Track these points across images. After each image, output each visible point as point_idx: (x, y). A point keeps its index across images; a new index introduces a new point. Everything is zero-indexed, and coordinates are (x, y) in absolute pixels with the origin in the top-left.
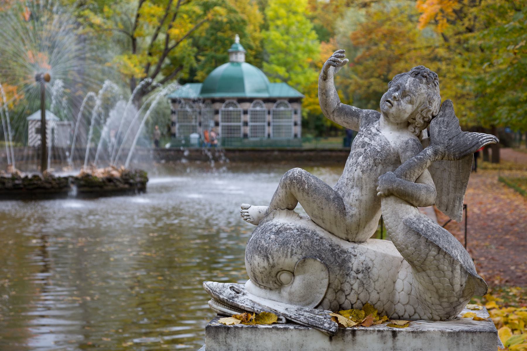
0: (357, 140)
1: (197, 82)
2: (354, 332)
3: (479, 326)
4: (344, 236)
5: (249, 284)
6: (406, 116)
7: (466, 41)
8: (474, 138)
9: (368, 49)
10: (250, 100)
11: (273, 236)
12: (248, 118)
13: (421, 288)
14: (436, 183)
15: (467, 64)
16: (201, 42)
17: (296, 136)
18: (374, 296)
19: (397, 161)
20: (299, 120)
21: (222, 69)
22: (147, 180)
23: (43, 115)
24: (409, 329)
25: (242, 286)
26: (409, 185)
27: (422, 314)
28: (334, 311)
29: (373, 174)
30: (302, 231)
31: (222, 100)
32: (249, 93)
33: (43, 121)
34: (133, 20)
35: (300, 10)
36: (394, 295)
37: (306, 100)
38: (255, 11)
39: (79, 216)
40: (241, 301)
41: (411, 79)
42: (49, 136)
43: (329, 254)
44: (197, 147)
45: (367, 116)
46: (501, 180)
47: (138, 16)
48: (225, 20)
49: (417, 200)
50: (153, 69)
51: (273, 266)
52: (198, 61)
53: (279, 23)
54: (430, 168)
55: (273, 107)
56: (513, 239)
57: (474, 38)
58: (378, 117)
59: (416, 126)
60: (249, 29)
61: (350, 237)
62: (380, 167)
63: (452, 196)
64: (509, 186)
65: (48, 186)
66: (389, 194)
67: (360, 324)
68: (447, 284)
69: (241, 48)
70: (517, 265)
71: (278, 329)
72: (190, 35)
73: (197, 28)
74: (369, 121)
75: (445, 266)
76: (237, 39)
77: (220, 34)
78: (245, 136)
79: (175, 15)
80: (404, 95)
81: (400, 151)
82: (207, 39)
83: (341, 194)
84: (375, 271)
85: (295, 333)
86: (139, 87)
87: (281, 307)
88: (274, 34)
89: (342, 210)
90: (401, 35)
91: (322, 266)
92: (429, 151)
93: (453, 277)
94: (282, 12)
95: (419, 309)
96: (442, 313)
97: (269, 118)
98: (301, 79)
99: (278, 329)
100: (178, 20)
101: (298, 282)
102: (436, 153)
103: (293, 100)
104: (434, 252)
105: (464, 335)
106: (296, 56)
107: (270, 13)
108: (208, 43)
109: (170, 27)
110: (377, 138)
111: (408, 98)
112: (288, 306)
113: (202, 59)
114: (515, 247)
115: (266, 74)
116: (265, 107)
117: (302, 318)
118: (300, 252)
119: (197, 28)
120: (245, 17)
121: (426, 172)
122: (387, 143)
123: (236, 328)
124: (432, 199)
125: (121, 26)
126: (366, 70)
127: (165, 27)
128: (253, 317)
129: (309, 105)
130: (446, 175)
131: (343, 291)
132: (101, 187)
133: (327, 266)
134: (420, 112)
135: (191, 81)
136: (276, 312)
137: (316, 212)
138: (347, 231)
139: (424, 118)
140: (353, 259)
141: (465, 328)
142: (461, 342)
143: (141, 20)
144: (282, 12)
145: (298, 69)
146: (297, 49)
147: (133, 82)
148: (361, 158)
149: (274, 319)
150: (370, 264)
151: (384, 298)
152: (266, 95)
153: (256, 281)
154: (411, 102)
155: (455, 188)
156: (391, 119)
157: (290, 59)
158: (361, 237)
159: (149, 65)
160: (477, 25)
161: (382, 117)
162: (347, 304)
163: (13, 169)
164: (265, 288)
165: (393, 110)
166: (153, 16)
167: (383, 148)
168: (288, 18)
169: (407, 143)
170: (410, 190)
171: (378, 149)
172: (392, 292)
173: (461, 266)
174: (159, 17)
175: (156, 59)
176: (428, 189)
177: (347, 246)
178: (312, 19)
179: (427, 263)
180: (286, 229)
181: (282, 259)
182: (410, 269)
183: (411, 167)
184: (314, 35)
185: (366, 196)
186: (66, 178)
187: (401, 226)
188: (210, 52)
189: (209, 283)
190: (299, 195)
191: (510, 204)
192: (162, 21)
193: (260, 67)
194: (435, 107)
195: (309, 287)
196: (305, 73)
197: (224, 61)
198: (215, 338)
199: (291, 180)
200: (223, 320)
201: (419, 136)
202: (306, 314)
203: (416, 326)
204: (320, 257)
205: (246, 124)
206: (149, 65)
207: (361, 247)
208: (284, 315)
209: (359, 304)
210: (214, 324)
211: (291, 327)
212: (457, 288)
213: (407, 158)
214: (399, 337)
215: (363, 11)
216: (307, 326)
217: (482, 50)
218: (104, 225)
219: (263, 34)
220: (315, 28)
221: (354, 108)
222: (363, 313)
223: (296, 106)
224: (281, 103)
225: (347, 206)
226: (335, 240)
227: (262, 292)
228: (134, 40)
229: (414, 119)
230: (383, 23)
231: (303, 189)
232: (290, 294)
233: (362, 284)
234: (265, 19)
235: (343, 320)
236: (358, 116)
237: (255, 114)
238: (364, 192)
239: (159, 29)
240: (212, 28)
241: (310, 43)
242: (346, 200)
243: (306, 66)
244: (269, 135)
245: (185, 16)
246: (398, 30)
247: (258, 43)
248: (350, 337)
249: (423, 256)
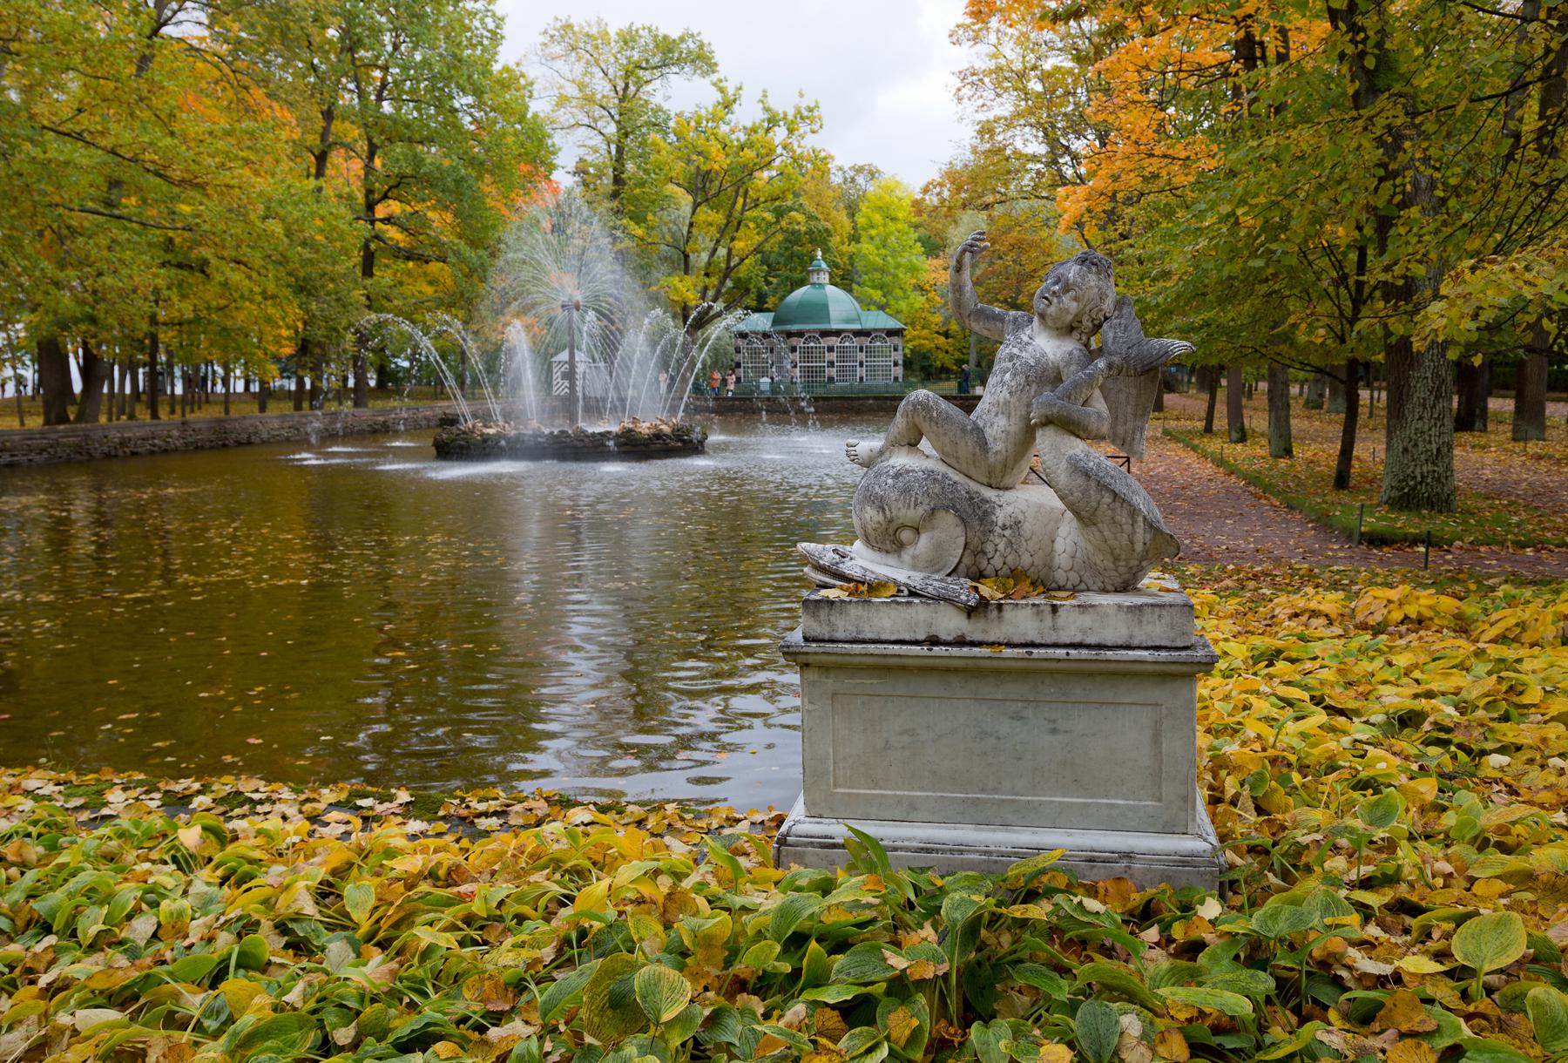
0: (1003, 352)
1: (768, 310)
2: (1000, 607)
3: (1168, 598)
4: (985, 480)
5: (858, 544)
6: (1070, 317)
7: (1120, 251)
8: (1161, 346)
9: (992, 264)
10: (837, 333)
11: (890, 481)
12: (833, 356)
13: (1089, 547)
14: (1110, 409)
15: (1121, 283)
16: (772, 258)
17: (896, 379)
18: (1026, 560)
19: (1057, 379)
20: (900, 358)
21: (800, 293)
23: (572, 355)
24: (1074, 602)
25: (848, 548)
26: (1075, 409)
27: (1090, 583)
28: (973, 579)
29: (1024, 397)
30: (929, 473)
31: (800, 334)
32: (835, 326)
33: (572, 362)
34: (685, 232)
35: (901, 215)
36: (1052, 559)
37: (910, 333)
38: (843, 217)
39: (621, 480)
40: (847, 568)
41: (1076, 268)
42: (579, 383)
43: (966, 504)
44: (768, 395)
45: (1016, 319)
46: (1166, 433)
47: (691, 225)
48: (803, 229)
49: (1085, 430)
50: (711, 293)
51: (891, 521)
52: (768, 283)
53: (873, 232)
54: (1101, 388)
55: (866, 341)
56: (1186, 505)
57: (1131, 246)
58: (1031, 321)
60: (834, 241)
61: (993, 482)
62: (1034, 387)
63: (1130, 425)
64: (1178, 441)
65: (579, 444)
66: (1048, 422)
67: (1008, 596)
68: (1125, 542)
69: (824, 265)
70: (1193, 537)
71: (898, 603)
72: (758, 250)
73: (767, 240)
74: (1018, 326)
75: (1123, 518)
76: (819, 253)
77: (796, 248)
78: (831, 379)
79: (739, 223)
80: (1067, 288)
81: (1062, 365)
82: (781, 255)
83: (981, 424)
84: (1027, 527)
85: (921, 608)
86: (693, 314)
87: (901, 575)
88: (866, 247)
89: (983, 444)
90: (1033, 245)
91: (956, 520)
92: (1101, 364)
93: (1134, 532)
94: (878, 218)
95: (1087, 576)
96: (1118, 581)
97: (861, 356)
98: (903, 305)
99: (898, 603)
100: (742, 228)
101: (924, 541)
102: (1110, 366)
103: (891, 333)
104: (1107, 499)
105: (1149, 610)
106: (895, 276)
107: (861, 220)
108: (782, 260)
109: (733, 239)
110: (1030, 348)
111: (1072, 293)
112: (912, 573)
113: (774, 280)
114: (1189, 515)
115: (856, 298)
116: (857, 341)
117: (930, 589)
118: (926, 501)
119: (767, 240)
120: (830, 226)
121: (1097, 393)
122: (1044, 355)
123: (843, 602)
124: (1105, 429)
125: (669, 238)
126: (988, 291)
127: (726, 240)
128: (864, 588)
129: (914, 338)
130: (1122, 397)
131: (985, 553)
132: (647, 446)
133: (962, 520)
135: (759, 309)
136: (895, 582)
137: (948, 449)
138: (990, 474)
140: (998, 511)
141: (1150, 600)
142: (1144, 619)
143: (695, 230)
144: (878, 218)
145: (900, 293)
146: (898, 266)
147: (685, 310)
148: (1008, 376)
149: (893, 591)
150: (1021, 517)
151: (1038, 561)
152: (857, 326)
153: (867, 541)
154: (1076, 299)
155: (1135, 415)
156: (1049, 322)
157: (888, 279)
158: (1007, 481)
159: (706, 288)
160: (1135, 230)
161: (1036, 319)
162: (989, 570)
163: (534, 424)
164: (880, 550)
165: (1052, 309)
166: (711, 225)
167: (1038, 362)
168: (885, 225)
169: (1071, 354)
170: (1075, 416)
171: (1032, 362)
172: (1050, 555)
173: (1145, 518)
174: (718, 227)
175: (714, 281)
176: (1099, 415)
177: (989, 494)
178: (916, 227)
179: (1099, 513)
180: (908, 472)
181: (903, 511)
182: (1075, 523)
183: (1076, 386)
184: (919, 248)
185: (1015, 426)
186: (602, 435)
187: (1064, 465)
188: (784, 272)
189: (805, 544)
190: (925, 426)
191: (1179, 462)
192: (722, 232)
193: (850, 291)
194: (1108, 305)
195: (939, 548)
196: (907, 298)
197: (802, 283)
198: (814, 615)
199: (914, 406)
200: (824, 593)
201: (1087, 345)
202: (936, 584)
203: (1083, 598)
204: (954, 507)
205: (831, 364)
206: (706, 288)
207: (1007, 496)
208: (906, 585)
209: (1005, 570)
210: (813, 597)
211: (917, 601)
212: (1139, 547)
213: (1072, 374)
214: (1061, 612)
215: (984, 215)
216: (938, 598)
217: (1141, 262)
219: (853, 248)
220: (919, 240)
221: (997, 310)
222: (1012, 582)
223: (896, 340)
225: (990, 440)
226: (974, 486)
227: (876, 556)
228: (686, 257)
230: (1010, 229)
231: (931, 418)
232: (914, 557)
233: (1010, 543)
234: (854, 228)
235: (985, 590)
236: (1002, 320)
237: (843, 350)
238: (1012, 421)
239: (718, 241)
240: (786, 240)
241: (914, 259)
242: (988, 432)
243: (909, 289)
245: (752, 225)
246: (1029, 237)
247: (845, 259)
248: (995, 613)
249: (1094, 504)
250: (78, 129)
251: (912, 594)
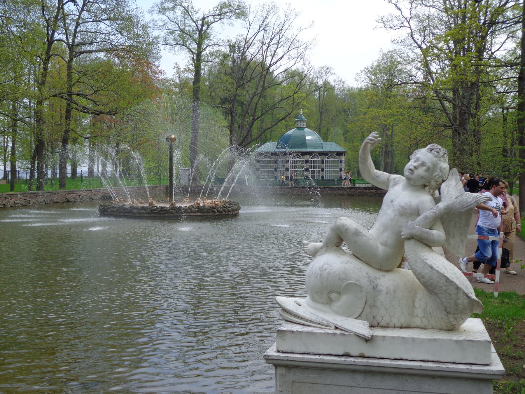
22: (239, 208)
55: (325, 158)
59: (431, 188)
103: (339, 154)
134: (433, 178)
139: (437, 182)
152: (321, 150)
218: (322, 83)
224: (331, 155)
229: (429, 182)
244: (323, 177)
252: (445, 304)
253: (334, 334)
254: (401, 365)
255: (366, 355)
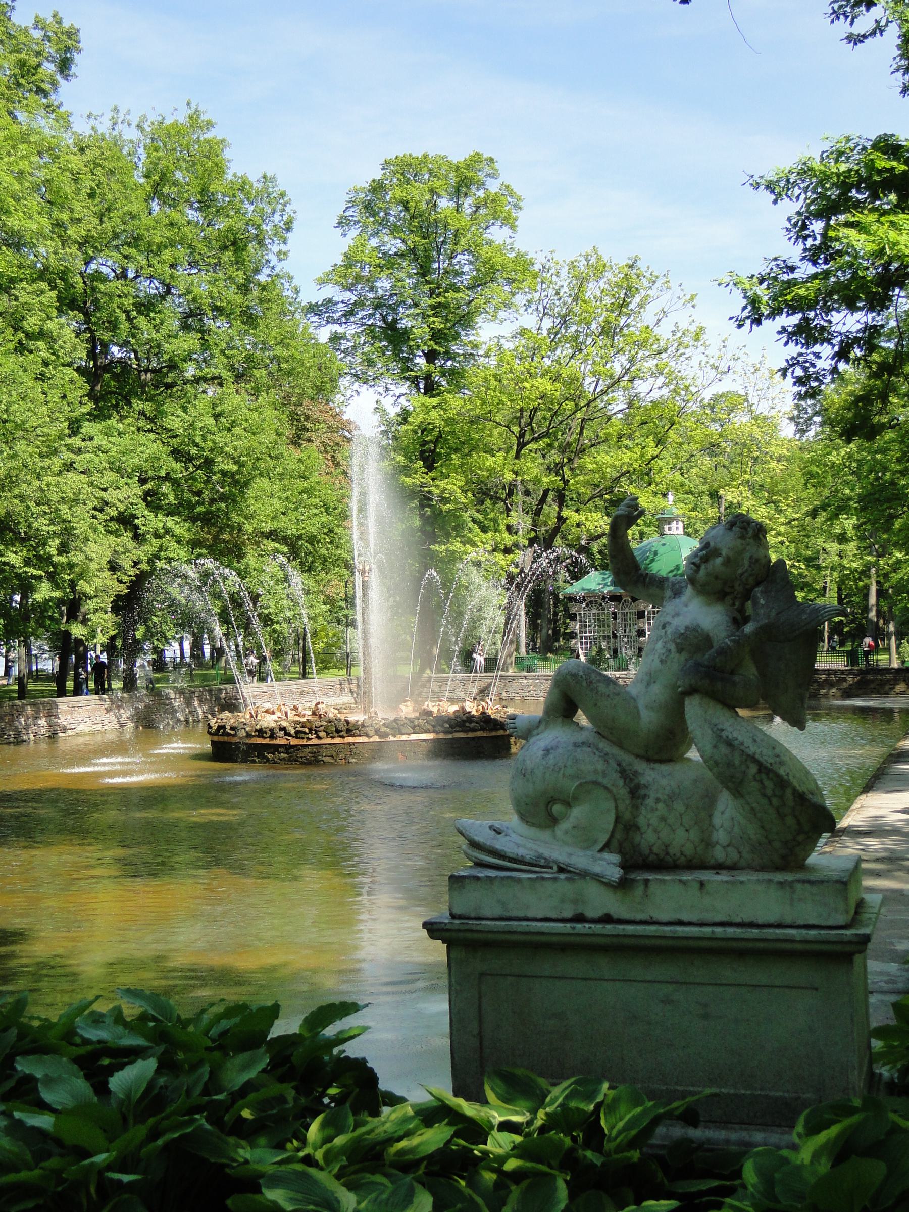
71: (543, 878)
87: (558, 853)
101: (577, 813)
173: (795, 790)
250: (292, 531)
251: (561, 870)
252: (759, 815)
253: (555, 879)
254: (676, 932)
255: (615, 916)
